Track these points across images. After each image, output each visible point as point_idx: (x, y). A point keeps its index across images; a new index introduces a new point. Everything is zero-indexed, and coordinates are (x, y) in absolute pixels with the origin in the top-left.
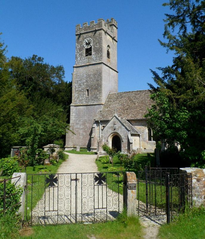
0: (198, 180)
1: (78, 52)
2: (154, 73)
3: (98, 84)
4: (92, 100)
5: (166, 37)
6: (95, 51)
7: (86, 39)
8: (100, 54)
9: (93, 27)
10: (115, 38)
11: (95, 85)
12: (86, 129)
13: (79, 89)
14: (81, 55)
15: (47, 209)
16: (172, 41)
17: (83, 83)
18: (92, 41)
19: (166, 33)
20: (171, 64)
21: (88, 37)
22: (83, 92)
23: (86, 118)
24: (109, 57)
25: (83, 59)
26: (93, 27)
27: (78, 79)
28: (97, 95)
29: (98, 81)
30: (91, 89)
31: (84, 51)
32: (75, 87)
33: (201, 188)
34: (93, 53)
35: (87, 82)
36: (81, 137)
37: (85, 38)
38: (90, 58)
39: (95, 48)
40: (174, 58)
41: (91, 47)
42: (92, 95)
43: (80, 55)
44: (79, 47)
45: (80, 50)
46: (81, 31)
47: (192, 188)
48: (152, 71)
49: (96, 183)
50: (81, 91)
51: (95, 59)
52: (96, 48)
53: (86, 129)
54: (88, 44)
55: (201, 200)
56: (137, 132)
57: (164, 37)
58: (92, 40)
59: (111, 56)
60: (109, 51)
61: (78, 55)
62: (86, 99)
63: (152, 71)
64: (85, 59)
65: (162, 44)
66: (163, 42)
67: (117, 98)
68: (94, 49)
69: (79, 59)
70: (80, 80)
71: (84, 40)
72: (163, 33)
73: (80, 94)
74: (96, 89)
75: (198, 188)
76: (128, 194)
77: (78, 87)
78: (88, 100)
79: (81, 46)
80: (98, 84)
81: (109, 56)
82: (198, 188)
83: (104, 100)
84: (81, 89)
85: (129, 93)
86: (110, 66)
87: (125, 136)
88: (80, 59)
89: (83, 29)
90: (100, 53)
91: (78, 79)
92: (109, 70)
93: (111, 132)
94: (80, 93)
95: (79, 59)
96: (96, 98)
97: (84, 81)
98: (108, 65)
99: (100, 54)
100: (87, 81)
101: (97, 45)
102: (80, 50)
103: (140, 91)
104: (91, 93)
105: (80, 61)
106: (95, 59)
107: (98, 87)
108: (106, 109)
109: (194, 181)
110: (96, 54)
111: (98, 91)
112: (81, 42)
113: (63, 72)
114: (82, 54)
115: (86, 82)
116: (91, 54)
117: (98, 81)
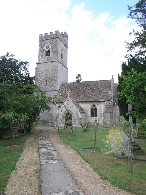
28: (53, 84)
31: (45, 53)
34: (51, 54)
43: (41, 55)
51: (52, 58)
68: (52, 51)
79: (42, 49)
96: (53, 86)
100: (46, 74)
116: (49, 55)
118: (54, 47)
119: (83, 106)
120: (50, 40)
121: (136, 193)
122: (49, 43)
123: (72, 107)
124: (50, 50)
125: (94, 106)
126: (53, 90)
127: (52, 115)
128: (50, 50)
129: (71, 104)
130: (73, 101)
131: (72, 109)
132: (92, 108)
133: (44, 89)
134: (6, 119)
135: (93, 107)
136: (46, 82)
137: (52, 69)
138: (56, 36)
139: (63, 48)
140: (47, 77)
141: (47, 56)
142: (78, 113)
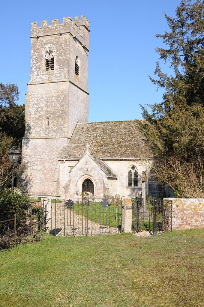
0: (177, 206)
1: (34, 64)
2: (143, 108)
3: (62, 111)
4: (55, 131)
5: (157, 74)
6: (59, 64)
7: (46, 46)
8: (65, 69)
9: (56, 28)
10: (86, 46)
11: (58, 112)
12: (45, 171)
13: (36, 116)
14: (39, 68)
15: (66, 224)
16: (162, 79)
17: (42, 108)
18: (55, 49)
19: (157, 70)
20: (160, 100)
21: (49, 43)
22: (41, 120)
23: (45, 156)
24: (77, 73)
25: (42, 74)
26: (56, 28)
27: (34, 102)
28: (61, 125)
29: (63, 106)
30: (53, 117)
31: (44, 62)
32: (30, 112)
33: (179, 212)
34: (56, 66)
35: (48, 107)
36: (38, 181)
37: (45, 44)
38: (52, 74)
39: (59, 59)
40: (164, 94)
41: (54, 57)
42: (54, 125)
43: (37, 67)
44: (36, 57)
45: (38, 60)
46: (38, 33)
47: (171, 212)
48: (141, 106)
49: (101, 206)
50: (38, 119)
51: (58, 75)
52: (60, 60)
53: (45, 171)
54: (50, 52)
55: (179, 221)
56: (114, 176)
57: (155, 74)
58: (54, 47)
59: (80, 71)
60: (77, 65)
61: (34, 67)
62: (46, 131)
63: (141, 106)
64: (44, 74)
65: (154, 81)
66: (153, 79)
67: (88, 131)
68: (57, 61)
69: (36, 73)
70: (37, 104)
71: (43, 47)
72: (155, 70)
73: (37, 123)
74: (60, 116)
75: (177, 212)
76: (126, 214)
77: (34, 113)
78: (48, 131)
79: (38, 55)
80: (62, 111)
81: (77, 71)
82: (177, 212)
83: (71, 132)
84: (38, 116)
85: (104, 124)
86: (78, 86)
87: (100, 180)
88: (37, 73)
89: (42, 31)
90: (66, 67)
91: (34, 102)
92: (78, 91)
93: (81, 175)
94: (37, 121)
95: (36, 73)
96: (60, 129)
97: (43, 105)
98: (77, 84)
99: (65, 69)
100: (47, 106)
101: (62, 56)
102: (38, 60)
103: (119, 122)
104: (53, 122)
105: (38, 77)
106: (58, 75)
107: (62, 114)
108: (74, 145)
109: (174, 207)
110: (60, 68)
111: (62, 119)
112: (38, 49)
113: (17, 93)
114: (40, 67)
115: (45, 107)
116: (52, 68)
117: (63, 106)
118: (61, 53)
119: (113, 166)
120: (53, 37)
121: (1, 175)
122: (52, 43)
123: (94, 169)
124: (53, 59)
125: (133, 167)
126: (60, 137)
127: (59, 183)
128: (53, 59)
129: (92, 164)
130: (95, 157)
131: (93, 172)
132: (130, 171)
133: (43, 135)
134: (88, 192)
135: (131, 170)
136: (46, 122)
137: (58, 97)
138: (65, 30)
139: (80, 53)
140: (48, 112)
141: (47, 69)
142: (103, 180)
